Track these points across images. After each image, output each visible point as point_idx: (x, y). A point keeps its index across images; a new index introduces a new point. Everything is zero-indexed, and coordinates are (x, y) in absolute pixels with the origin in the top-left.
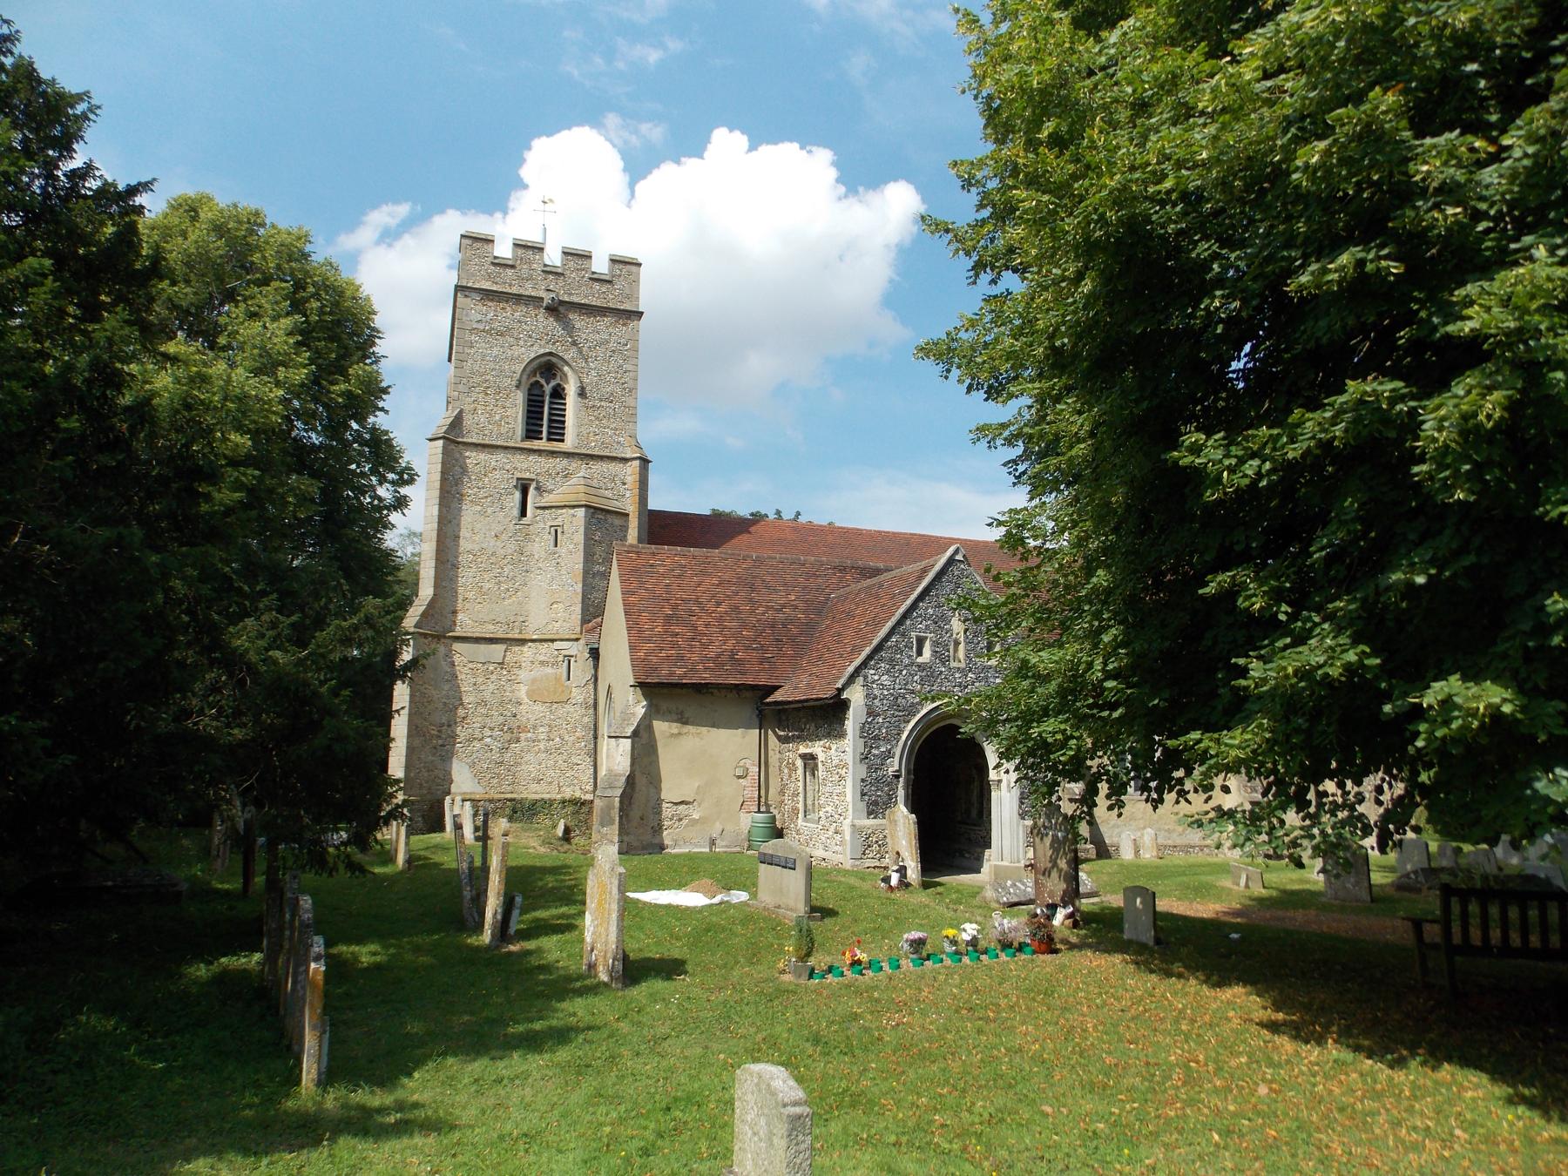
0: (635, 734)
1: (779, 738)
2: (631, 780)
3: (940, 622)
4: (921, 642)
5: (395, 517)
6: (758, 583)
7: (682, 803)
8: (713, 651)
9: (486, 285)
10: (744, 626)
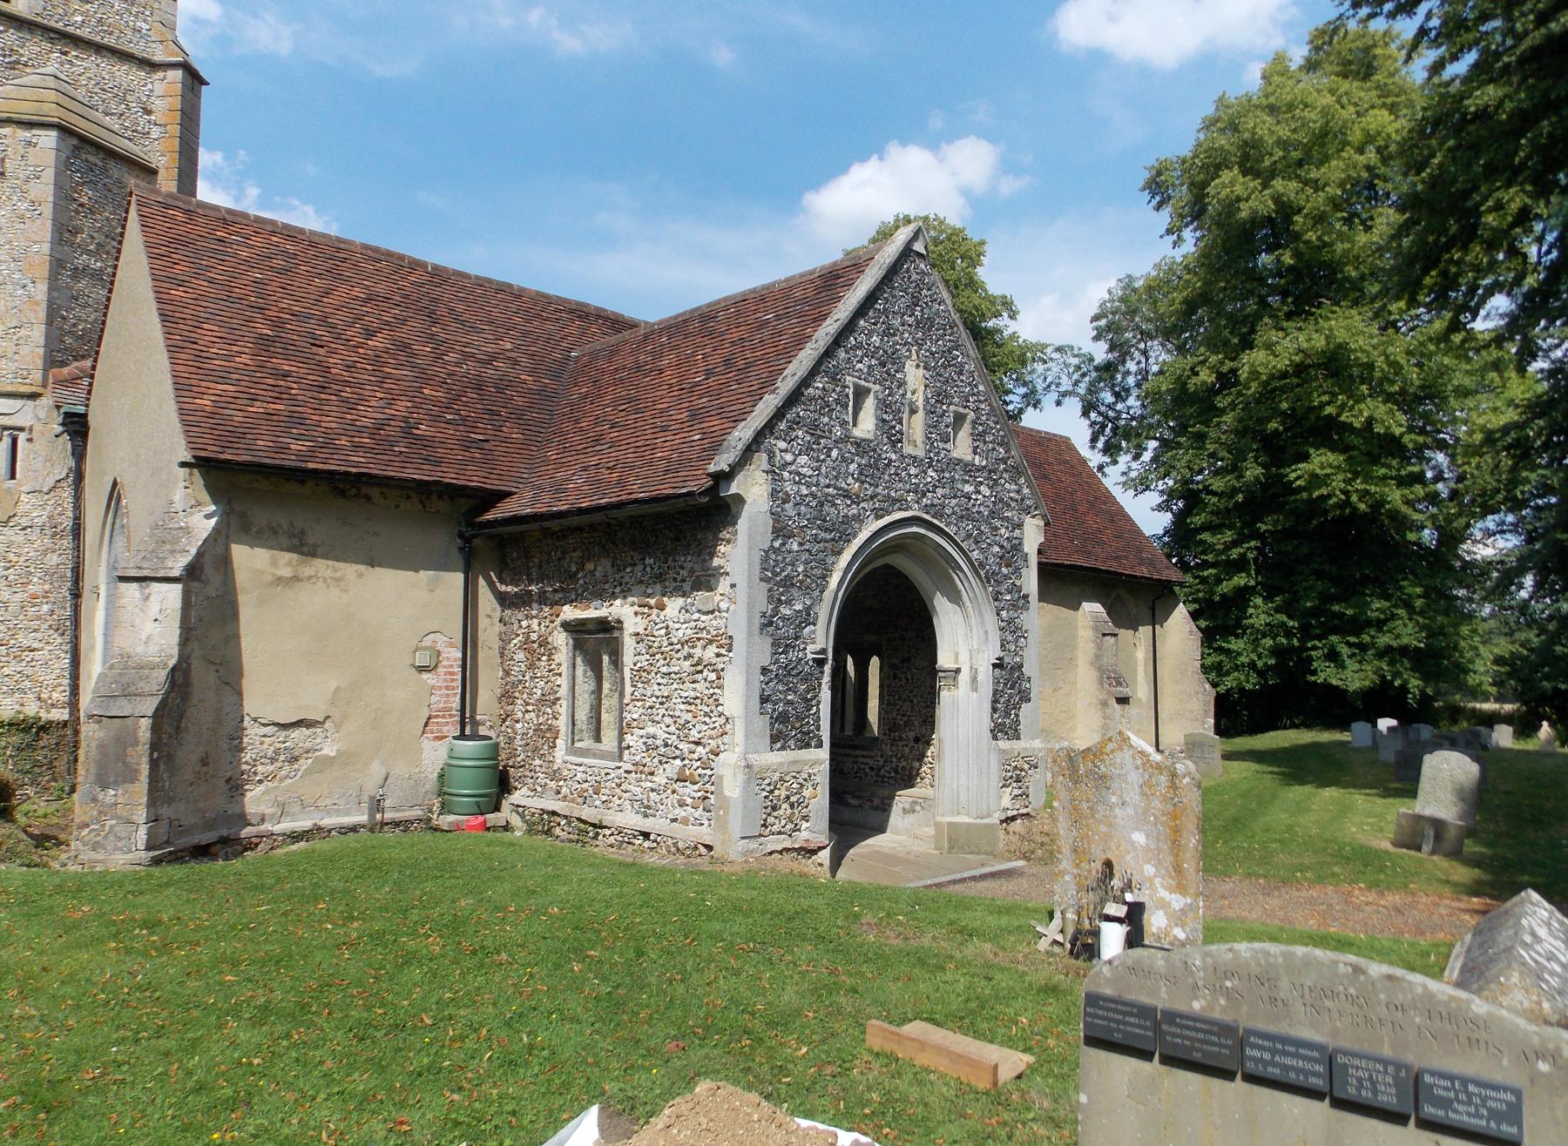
0: (192, 573)
1: (503, 600)
2: (180, 679)
3: (889, 363)
4: (861, 394)
6: (442, 311)
7: (299, 723)
8: (368, 415)
10: (425, 378)
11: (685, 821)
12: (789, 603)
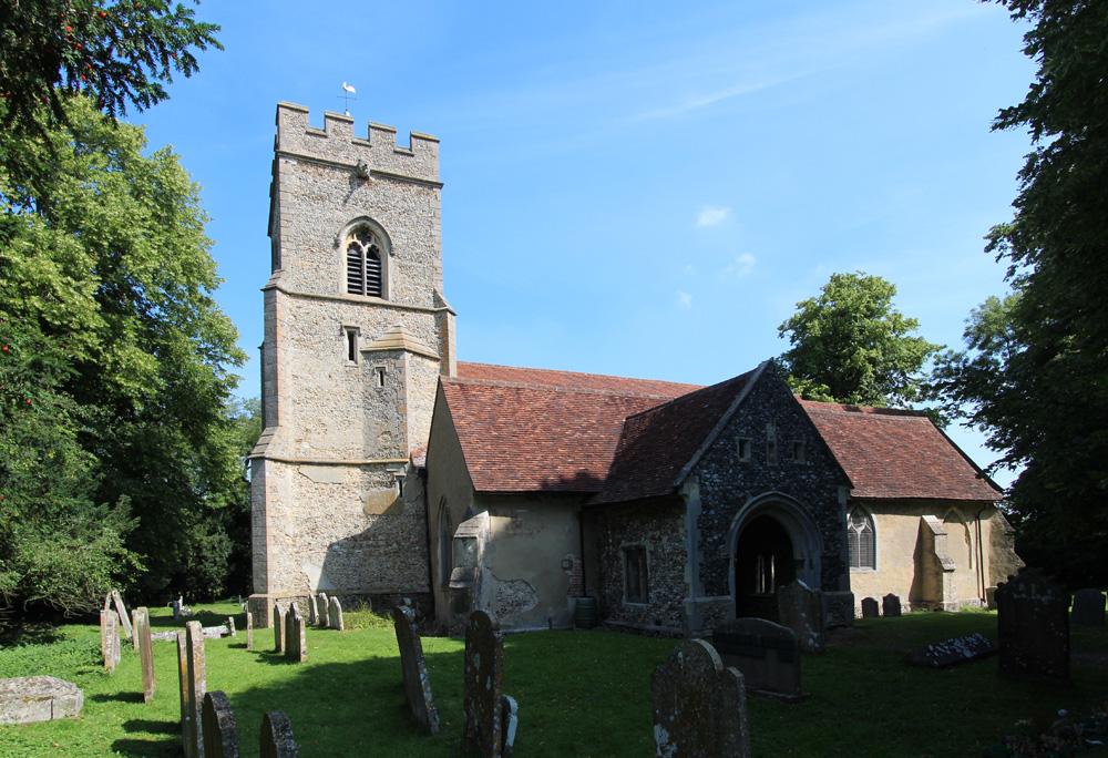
4: (742, 443)
5: (233, 391)
9: (304, 153)
11: (673, 626)
12: (711, 536)
